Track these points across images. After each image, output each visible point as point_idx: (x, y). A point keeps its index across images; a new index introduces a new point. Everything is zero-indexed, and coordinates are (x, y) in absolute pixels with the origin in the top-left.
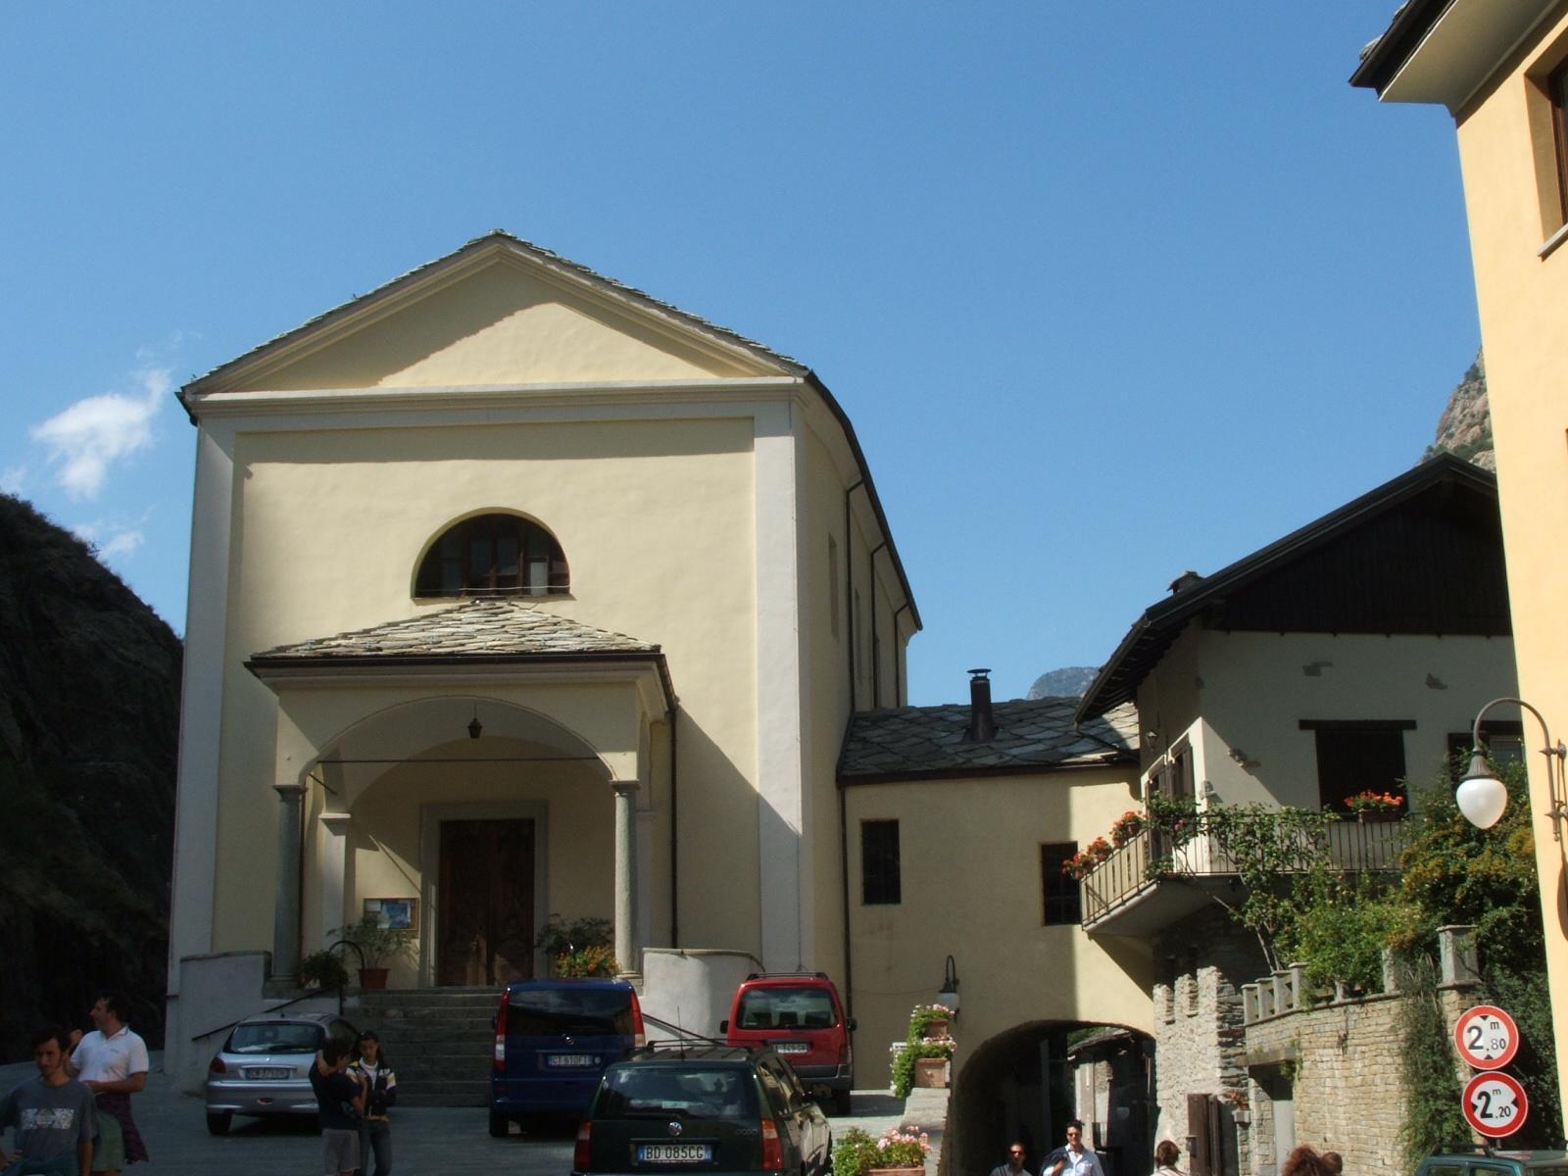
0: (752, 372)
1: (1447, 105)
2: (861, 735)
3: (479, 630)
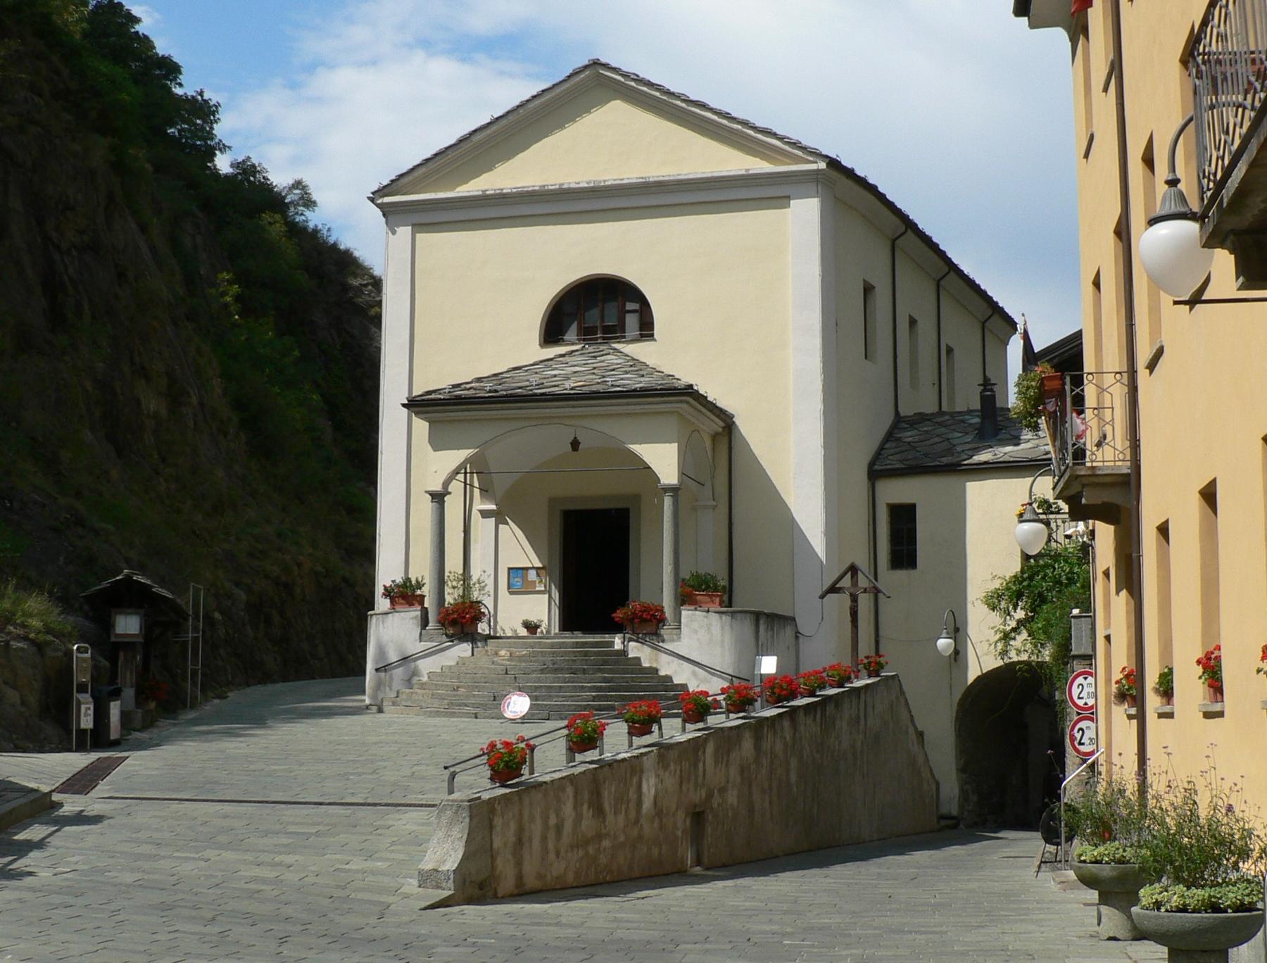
0: (788, 161)
1: (1063, 27)
2: (899, 435)
3: (575, 372)
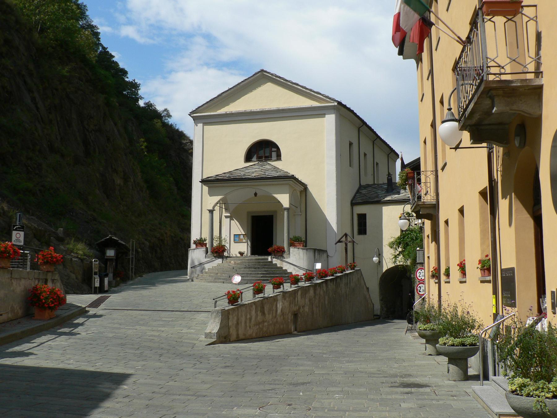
2: (361, 191)
